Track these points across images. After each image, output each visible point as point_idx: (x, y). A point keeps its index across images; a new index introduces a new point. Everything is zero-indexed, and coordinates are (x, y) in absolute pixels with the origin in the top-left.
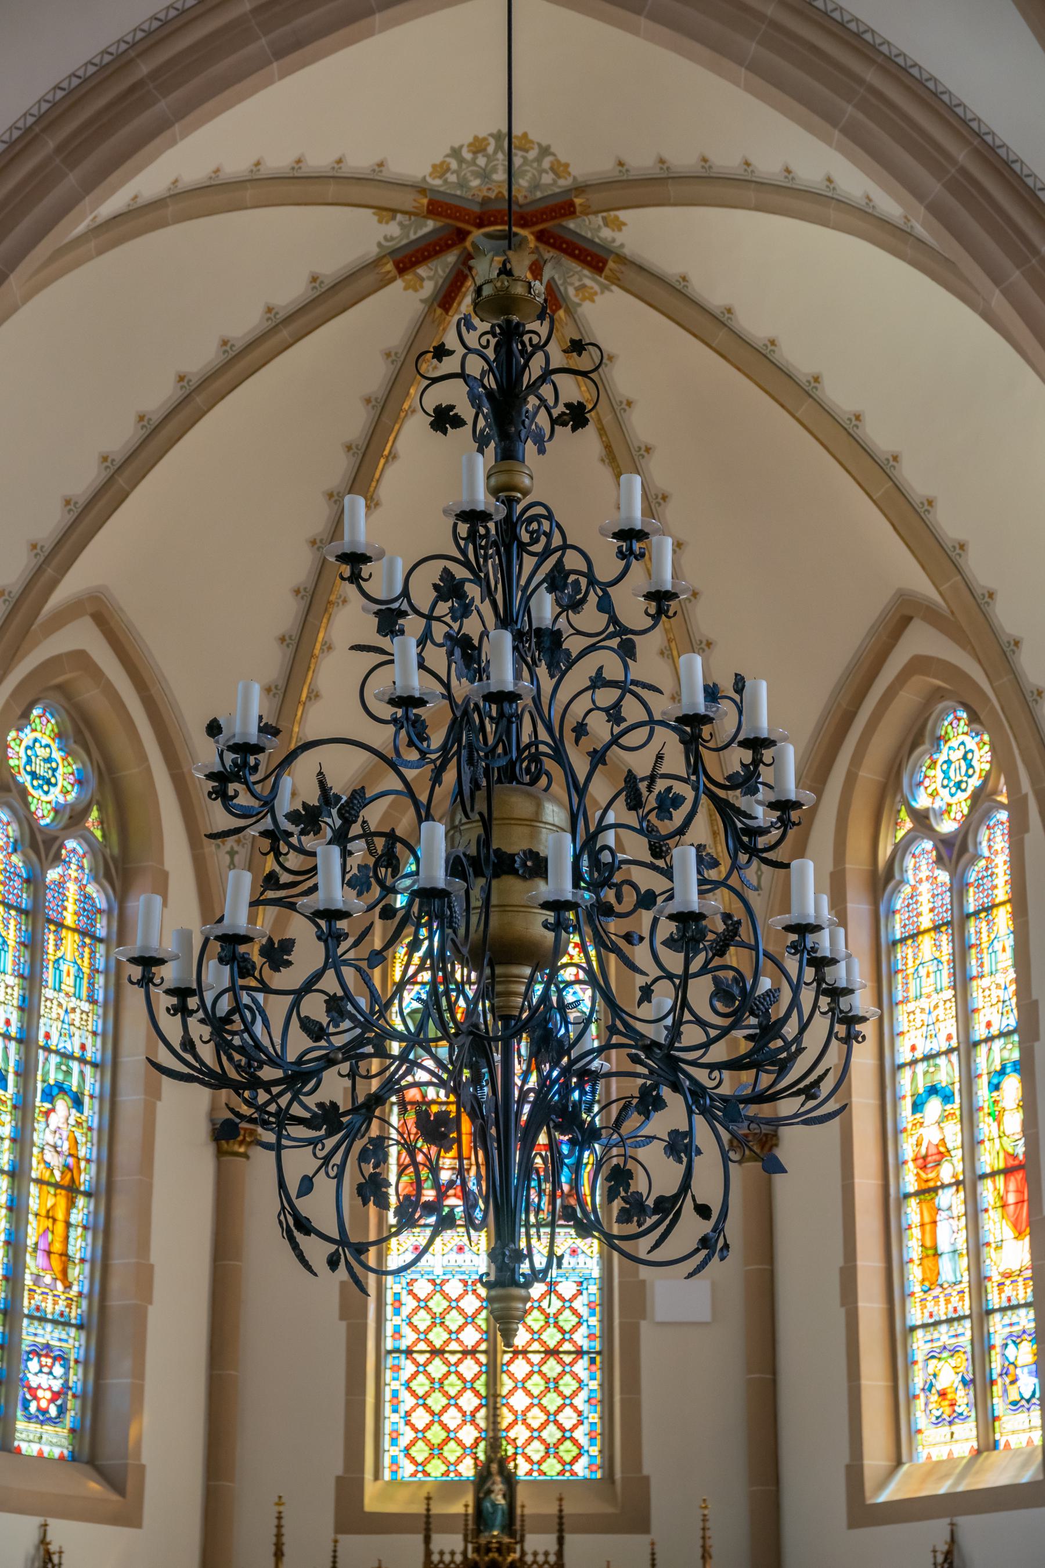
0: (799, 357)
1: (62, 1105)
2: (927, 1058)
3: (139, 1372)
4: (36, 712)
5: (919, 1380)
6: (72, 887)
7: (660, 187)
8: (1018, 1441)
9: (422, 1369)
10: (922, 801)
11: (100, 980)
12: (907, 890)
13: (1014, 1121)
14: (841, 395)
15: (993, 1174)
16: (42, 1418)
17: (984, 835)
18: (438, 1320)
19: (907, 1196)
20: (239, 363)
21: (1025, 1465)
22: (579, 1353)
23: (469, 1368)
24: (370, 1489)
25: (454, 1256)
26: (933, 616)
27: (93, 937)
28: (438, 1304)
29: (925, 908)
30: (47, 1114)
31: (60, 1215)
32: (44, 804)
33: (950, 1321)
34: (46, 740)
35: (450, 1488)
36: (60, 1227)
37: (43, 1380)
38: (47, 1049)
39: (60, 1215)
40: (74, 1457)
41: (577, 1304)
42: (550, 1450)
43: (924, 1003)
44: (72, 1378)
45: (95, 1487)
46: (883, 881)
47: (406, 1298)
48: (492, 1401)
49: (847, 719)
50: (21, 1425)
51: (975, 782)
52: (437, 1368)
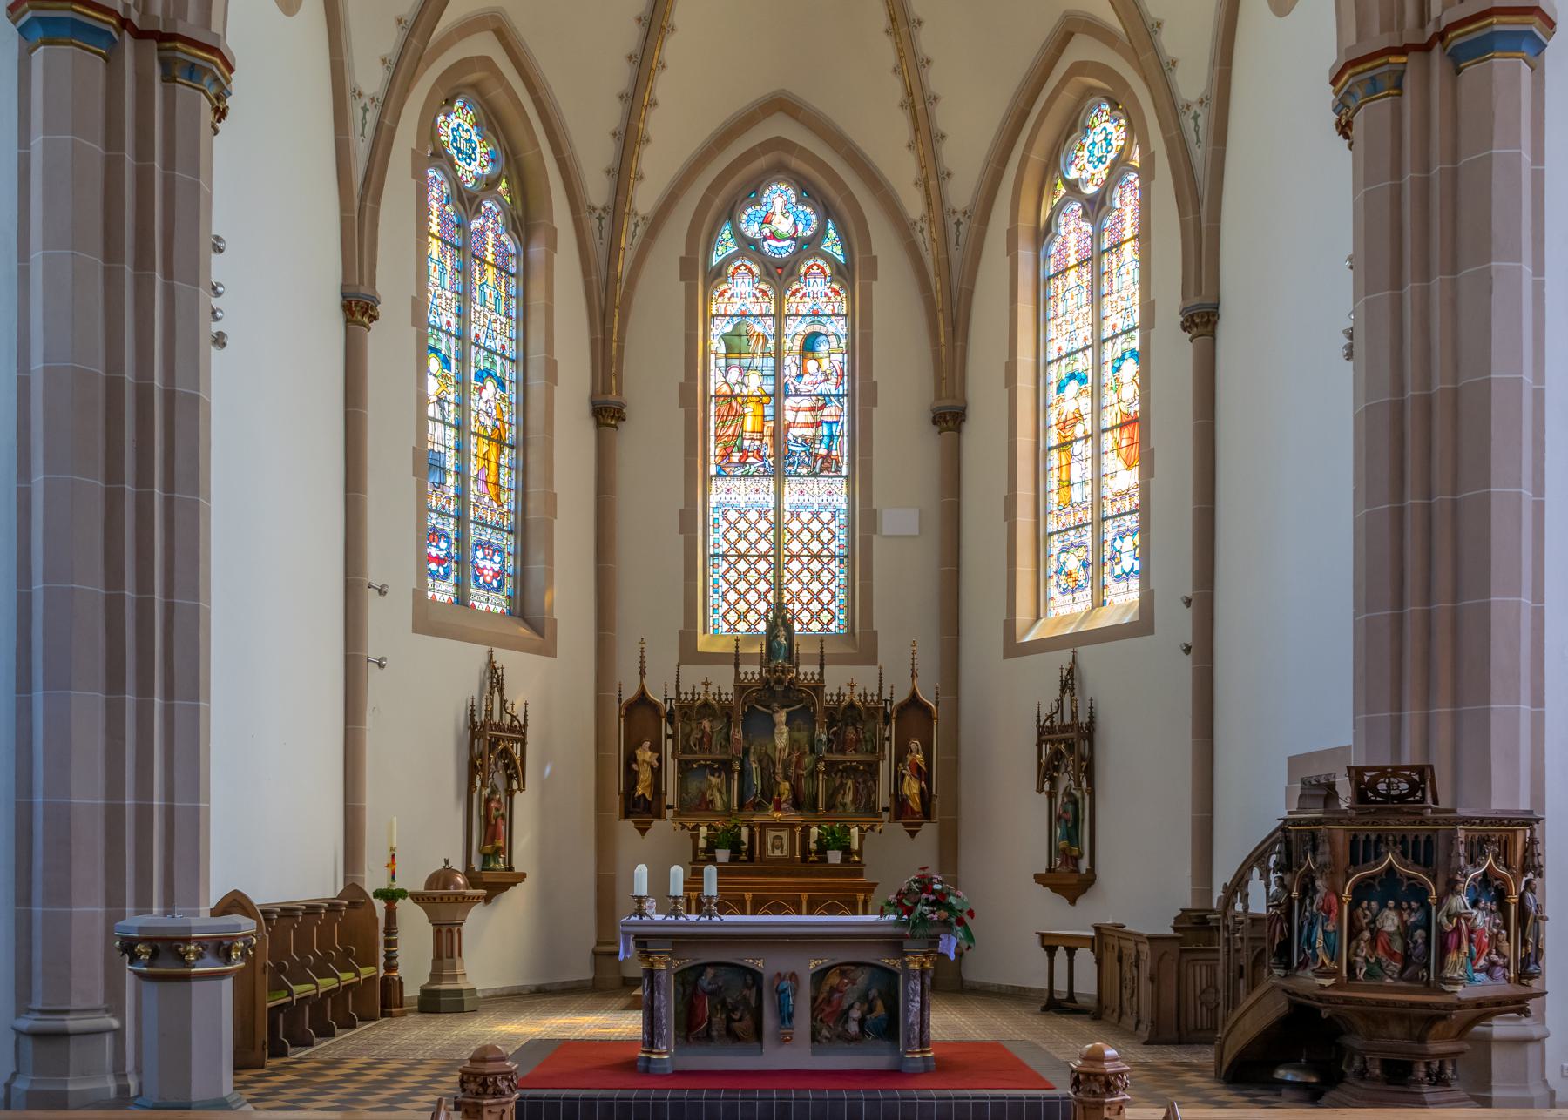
1: (490, 386)
2: (1069, 355)
3: (550, 561)
4: (458, 104)
5: (1053, 566)
6: (490, 235)
8: (1118, 600)
9: (733, 566)
10: (1073, 174)
11: (513, 302)
12: (1059, 240)
13: (1130, 392)
15: (1112, 429)
16: (487, 587)
17: (1117, 192)
18: (743, 536)
19: (1051, 449)
21: (1125, 613)
22: (833, 556)
23: (763, 566)
24: (701, 638)
25: (752, 496)
27: (507, 272)
28: (742, 526)
29: (1072, 252)
30: (481, 390)
31: (493, 458)
32: (472, 170)
33: (1076, 527)
34: (467, 126)
35: (751, 639)
36: (493, 466)
37: (488, 564)
38: (477, 345)
39: (493, 458)
40: (511, 613)
41: (832, 526)
42: (815, 616)
43: (1068, 317)
44: (507, 565)
45: (524, 631)
46: (1043, 234)
47: (722, 522)
48: (778, 586)
49: (1024, 115)
50: (473, 590)
51: (1112, 156)
52: (742, 566)
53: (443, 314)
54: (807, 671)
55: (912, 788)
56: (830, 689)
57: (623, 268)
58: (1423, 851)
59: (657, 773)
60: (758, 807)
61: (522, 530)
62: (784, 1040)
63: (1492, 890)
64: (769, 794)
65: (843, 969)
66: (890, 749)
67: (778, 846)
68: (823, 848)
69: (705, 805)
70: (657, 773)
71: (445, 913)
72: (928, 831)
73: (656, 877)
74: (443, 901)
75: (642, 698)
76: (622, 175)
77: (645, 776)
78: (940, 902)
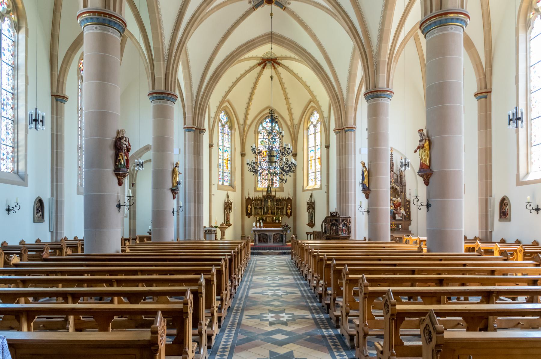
0: (300, 75)
7: (286, 58)
14: (304, 79)
20: (242, 76)
26: (314, 102)
32: (223, 122)
35: (265, 188)
46: (308, 129)
49: (305, 112)
53: (220, 143)
54: (273, 193)
55: (289, 211)
56: (276, 197)
57: (245, 133)
58: (337, 221)
59: (251, 209)
60: (266, 214)
61: (231, 173)
62: (270, 242)
63: (345, 225)
64: (268, 212)
65: (277, 234)
66: (285, 205)
67: (269, 220)
68: (275, 220)
69: (258, 214)
70: (251, 209)
71: (223, 229)
72: (291, 218)
73: (252, 223)
74: (222, 228)
75: (249, 198)
76: (245, 119)
77: (249, 210)
78: (287, 226)
